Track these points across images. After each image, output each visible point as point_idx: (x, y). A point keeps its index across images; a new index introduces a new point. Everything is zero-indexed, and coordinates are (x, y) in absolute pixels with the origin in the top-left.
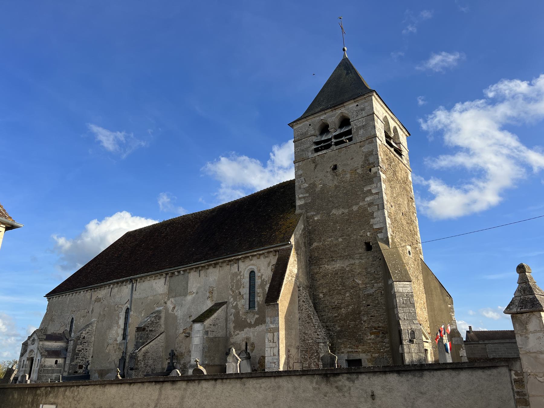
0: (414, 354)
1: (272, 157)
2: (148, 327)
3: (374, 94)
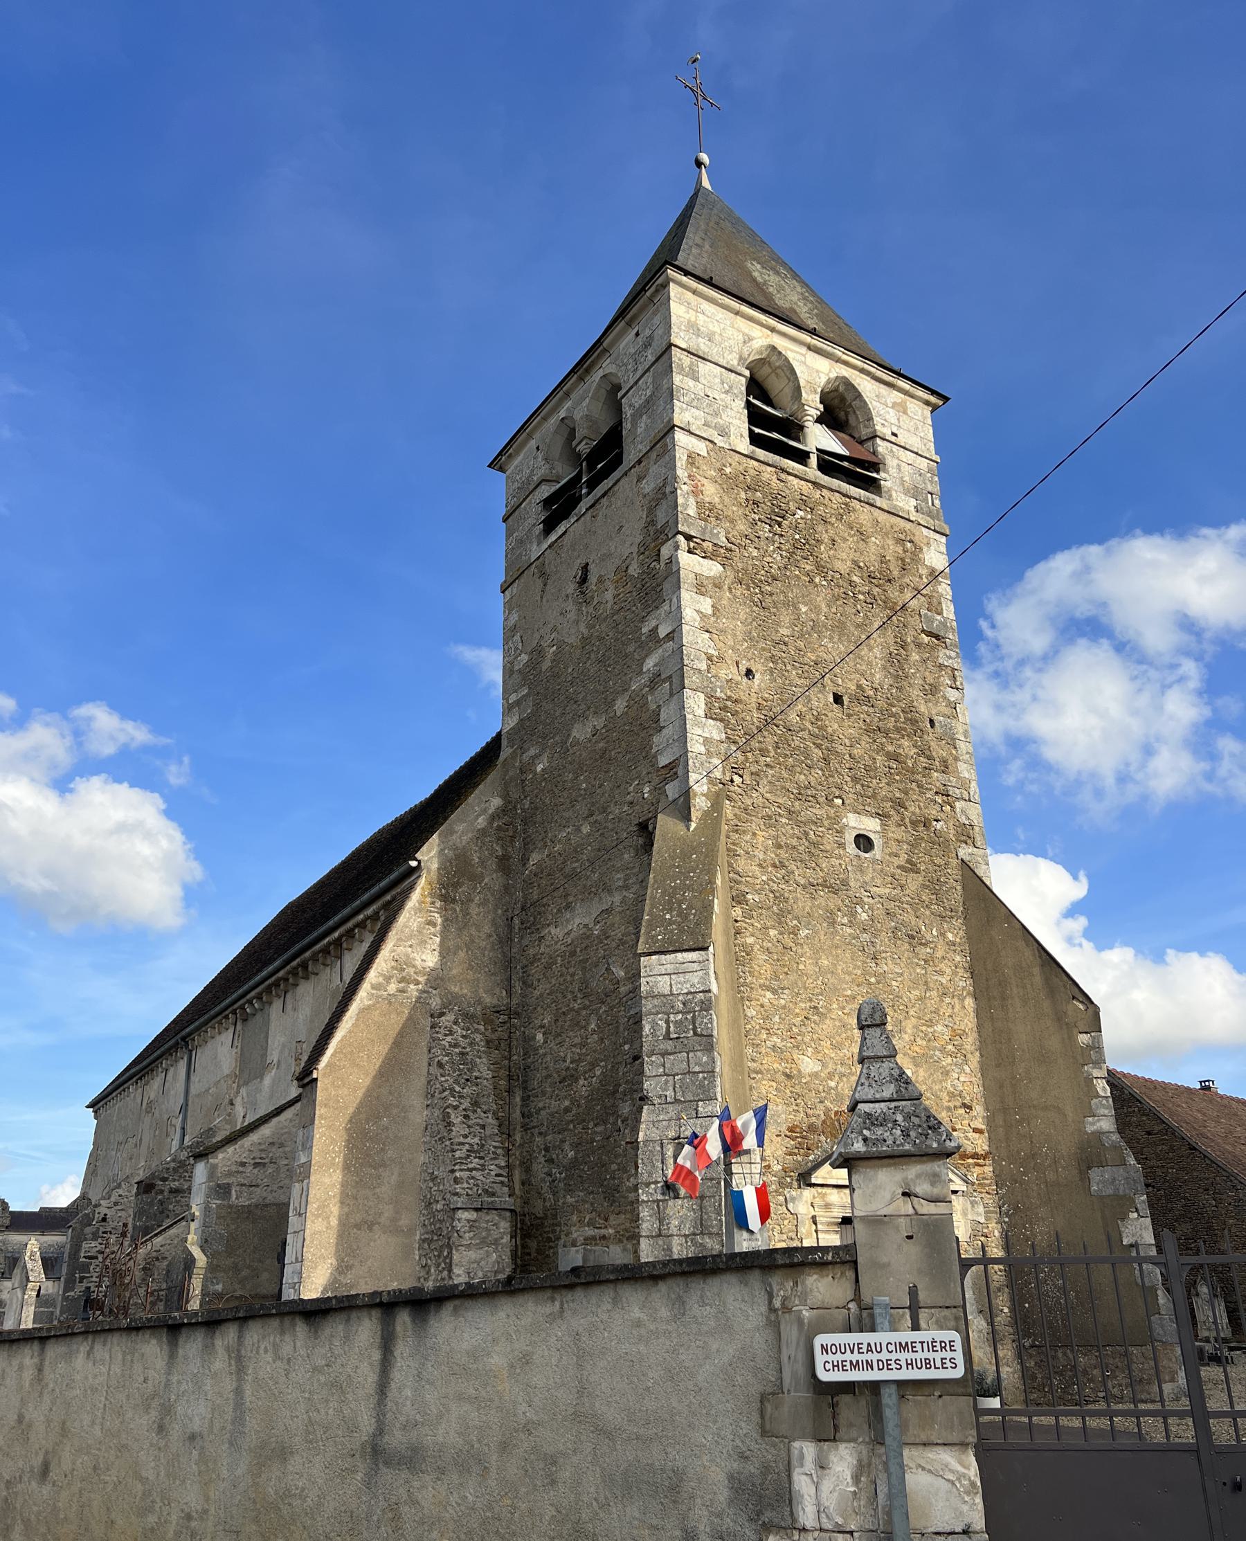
0: (676, 1241)
1: (989, 633)
2: (164, 1180)
3: (671, 272)
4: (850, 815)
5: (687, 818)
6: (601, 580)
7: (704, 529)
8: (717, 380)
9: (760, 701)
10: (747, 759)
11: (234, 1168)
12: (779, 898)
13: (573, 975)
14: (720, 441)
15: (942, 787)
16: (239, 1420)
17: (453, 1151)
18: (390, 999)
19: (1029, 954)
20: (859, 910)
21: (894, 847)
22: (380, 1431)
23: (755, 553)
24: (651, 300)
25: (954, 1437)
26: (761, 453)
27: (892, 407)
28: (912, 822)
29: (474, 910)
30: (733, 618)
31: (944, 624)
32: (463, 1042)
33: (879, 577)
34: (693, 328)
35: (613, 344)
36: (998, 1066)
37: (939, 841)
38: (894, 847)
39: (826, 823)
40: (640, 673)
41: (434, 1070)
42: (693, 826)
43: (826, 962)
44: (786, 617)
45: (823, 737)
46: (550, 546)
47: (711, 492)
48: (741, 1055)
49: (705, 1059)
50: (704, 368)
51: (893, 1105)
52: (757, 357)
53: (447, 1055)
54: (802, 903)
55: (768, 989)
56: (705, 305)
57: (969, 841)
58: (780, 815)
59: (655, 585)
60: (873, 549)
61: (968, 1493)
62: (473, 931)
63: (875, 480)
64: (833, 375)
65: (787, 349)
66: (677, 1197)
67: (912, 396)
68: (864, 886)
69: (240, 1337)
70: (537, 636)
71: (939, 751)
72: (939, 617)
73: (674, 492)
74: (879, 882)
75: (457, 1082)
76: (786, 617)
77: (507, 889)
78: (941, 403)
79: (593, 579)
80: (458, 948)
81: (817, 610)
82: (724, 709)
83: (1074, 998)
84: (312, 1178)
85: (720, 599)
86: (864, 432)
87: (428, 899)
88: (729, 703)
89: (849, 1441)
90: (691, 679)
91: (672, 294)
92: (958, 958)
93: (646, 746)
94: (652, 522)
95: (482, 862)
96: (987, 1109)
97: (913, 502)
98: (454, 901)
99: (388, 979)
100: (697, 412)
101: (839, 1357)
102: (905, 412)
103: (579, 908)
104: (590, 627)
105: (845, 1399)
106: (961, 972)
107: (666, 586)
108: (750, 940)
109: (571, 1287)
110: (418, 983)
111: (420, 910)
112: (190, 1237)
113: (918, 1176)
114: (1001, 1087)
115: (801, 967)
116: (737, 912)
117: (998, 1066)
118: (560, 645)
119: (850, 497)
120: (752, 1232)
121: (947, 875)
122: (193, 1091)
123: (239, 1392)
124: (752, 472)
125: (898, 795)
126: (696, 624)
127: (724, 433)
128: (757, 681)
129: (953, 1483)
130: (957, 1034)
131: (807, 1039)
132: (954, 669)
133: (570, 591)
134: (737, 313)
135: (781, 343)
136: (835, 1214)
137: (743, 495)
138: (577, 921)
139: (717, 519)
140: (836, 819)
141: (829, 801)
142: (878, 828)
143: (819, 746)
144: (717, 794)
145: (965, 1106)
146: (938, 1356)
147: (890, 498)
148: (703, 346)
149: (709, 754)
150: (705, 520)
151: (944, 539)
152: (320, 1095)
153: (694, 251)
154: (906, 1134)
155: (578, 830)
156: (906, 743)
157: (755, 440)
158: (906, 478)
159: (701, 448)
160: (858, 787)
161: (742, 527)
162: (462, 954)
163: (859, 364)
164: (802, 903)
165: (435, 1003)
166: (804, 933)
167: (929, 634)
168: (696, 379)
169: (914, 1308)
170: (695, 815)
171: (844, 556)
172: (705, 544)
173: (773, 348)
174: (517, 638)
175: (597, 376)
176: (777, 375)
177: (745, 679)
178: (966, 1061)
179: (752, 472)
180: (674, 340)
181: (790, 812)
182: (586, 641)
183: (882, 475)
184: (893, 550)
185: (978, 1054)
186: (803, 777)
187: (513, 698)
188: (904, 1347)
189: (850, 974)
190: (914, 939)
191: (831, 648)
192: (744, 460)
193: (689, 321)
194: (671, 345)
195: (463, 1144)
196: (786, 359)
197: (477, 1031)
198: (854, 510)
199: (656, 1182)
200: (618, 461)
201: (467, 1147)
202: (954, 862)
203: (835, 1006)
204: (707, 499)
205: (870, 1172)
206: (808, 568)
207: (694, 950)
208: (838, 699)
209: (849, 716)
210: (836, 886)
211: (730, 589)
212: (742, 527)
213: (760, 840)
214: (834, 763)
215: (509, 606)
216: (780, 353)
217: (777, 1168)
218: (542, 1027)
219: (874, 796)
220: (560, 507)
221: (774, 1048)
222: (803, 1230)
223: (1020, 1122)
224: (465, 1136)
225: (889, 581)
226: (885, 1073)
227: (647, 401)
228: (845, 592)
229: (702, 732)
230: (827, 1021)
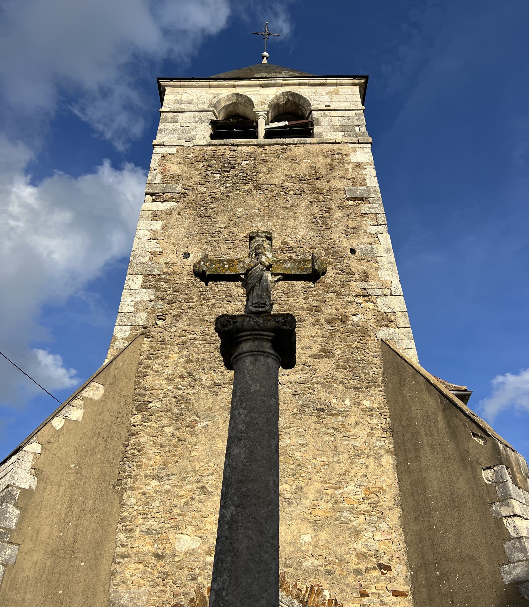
28: (327, 321)
37: (363, 331)
52: (228, 103)
55: (153, 477)
65: (245, 92)
67: (342, 85)
71: (356, 267)
88: (163, 277)
96: (411, 568)
106: (378, 433)
114: (421, 541)
115: (194, 453)
117: (416, 519)
124: (209, 152)
130: (372, 492)
132: (376, 214)
134: (210, 87)
135: (240, 91)
145: (381, 567)
149: (137, 310)
173: (237, 94)
178: (382, 518)
185: (398, 509)
190: (323, 411)
192: (205, 148)
196: (246, 97)
216: (241, 95)
221: (148, 531)
223: (439, 579)
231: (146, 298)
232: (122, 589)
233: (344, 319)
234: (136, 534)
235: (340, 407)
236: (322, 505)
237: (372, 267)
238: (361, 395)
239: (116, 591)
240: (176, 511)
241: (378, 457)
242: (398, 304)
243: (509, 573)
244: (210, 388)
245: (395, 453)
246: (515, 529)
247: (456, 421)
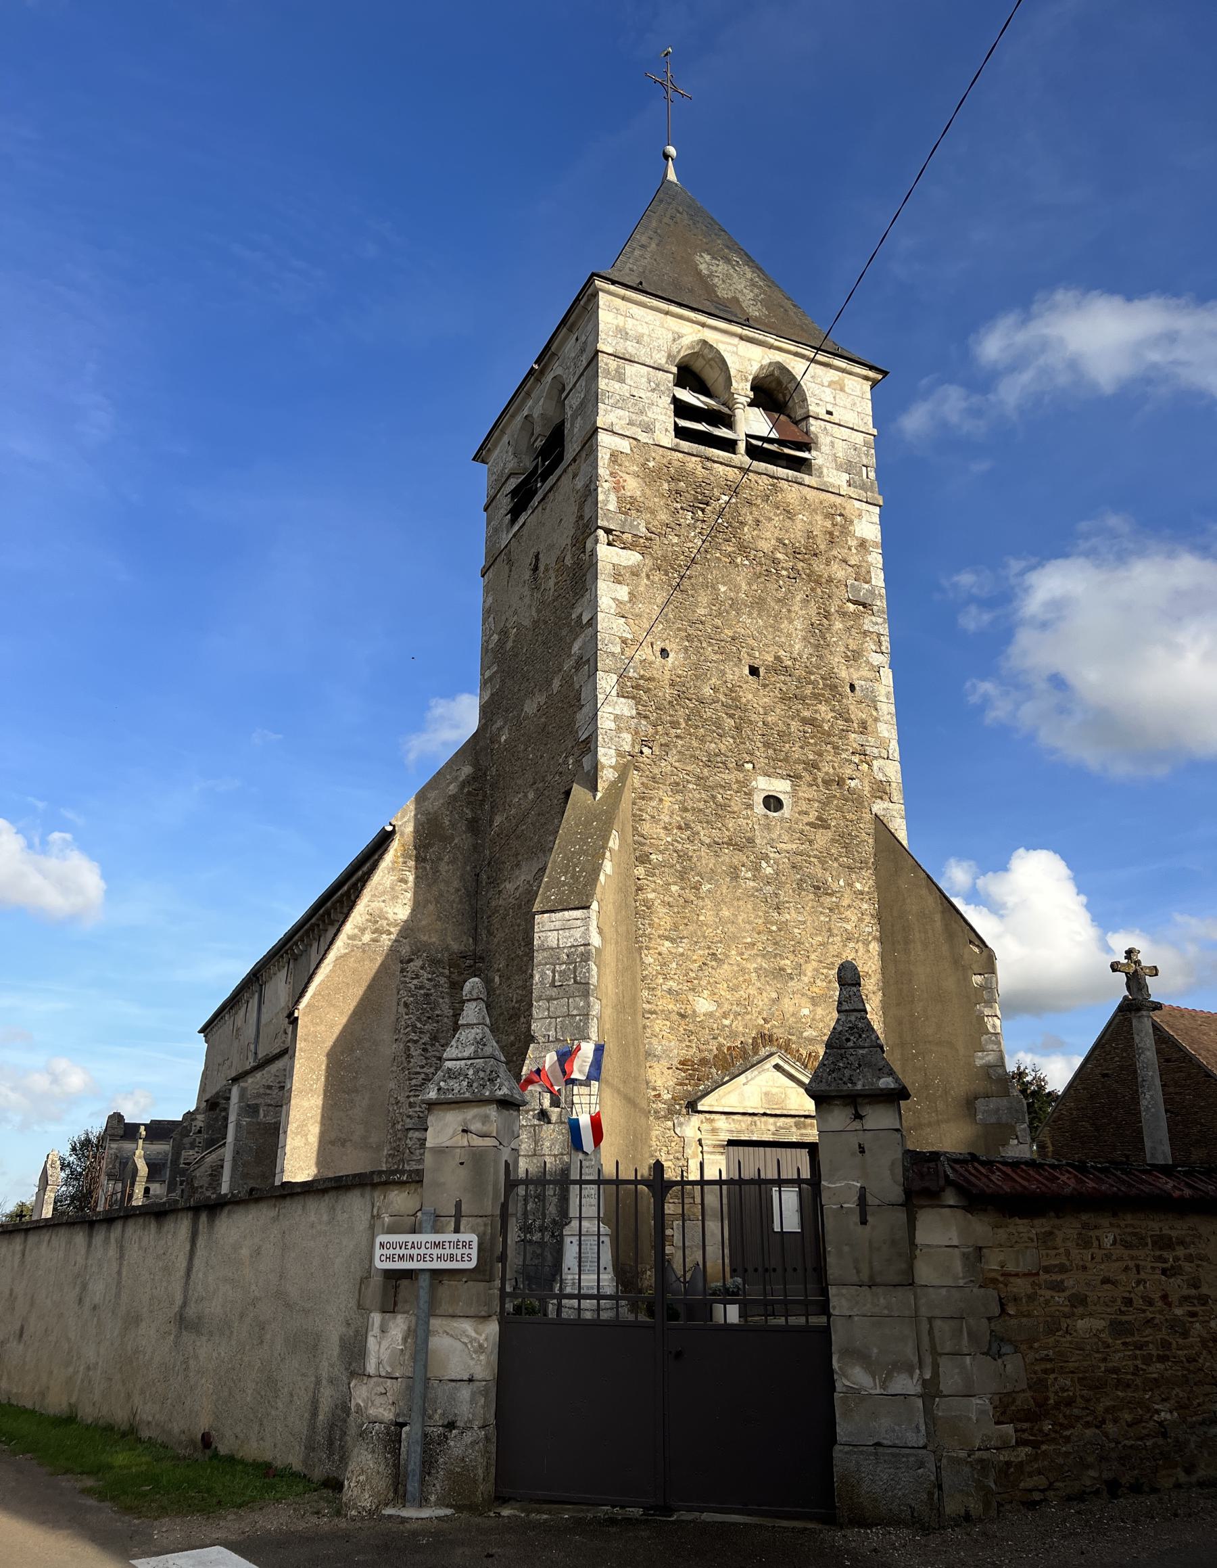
3: (598, 283)
4: (760, 778)
5: (594, 789)
6: (547, 570)
7: (624, 523)
8: (644, 380)
9: (674, 677)
10: (657, 733)
11: (262, 1091)
12: (683, 856)
13: (519, 925)
14: (644, 438)
15: (859, 748)
16: (118, 1295)
17: (410, 1079)
18: (364, 948)
19: (931, 901)
20: (764, 864)
21: (804, 806)
22: (185, 1304)
23: (675, 540)
24: (585, 308)
25: (472, 1312)
26: (685, 445)
27: (829, 386)
28: (824, 782)
29: (443, 867)
30: (650, 603)
31: (872, 592)
32: (428, 985)
33: (806, 552)
34: (623, 333)
35: (559, 348)
36: (898, 1005)
37: (856, 799)
38: (804, 806)
39: (735, 787)
40: (570, 656)
41: (402, 1010)
42: (599, 795)
43: (727, 913)
44: (704, 598)
45: (735, 706)
46: (514, 536)
47: (633, 486)
48: (634, 999)
49: (582, 1004)
50: (631, 369)
51: (470, 1062)
53: (412, 996)
54: (706, 860)
56: (635, 309)
57: (886, 797)
58: (688, 782)
59: (581, 576)
60: (799, 525)
61: (475, 1352)
62: (442, 886)
63: (805, 460)
64: (766, 362)
65: (718, 341)
66: (549, 1122)
67: (850, 373)
68: (771, 843)
69: (123, 1231)
70: (504, 618)
71: (857, 714)
72: (866, 586)
73: (596, 490)
74: (786, 839)
75: (419, 1019)
76: (704, 598)
77: (475, 848)
78: (880, 377)
79: (542, 568)
80: (428, 901)
81: (737, 588)
82: (637, 687)
83: (971, 942)
84: (293, 1102)
85: (637, 586)
86: (799, 413)
87: (401, 860)
88: (641, 682)
89: (404, 1313)
90: (603, 662)
91: (601, 303)
92: (865, 906)
93: (572, 721)
94: (581, 517)
95: (453, 825)
97: (846, 477)
98: (424, 860)
99: (363, 930)
100: (621, 412)
101: (391, 1251)
102: (842, 390)
103: (524, 868)
104: (539, 611)
105: (404, 1283)
106: (867, 919)
107: (589, 576)
108: (651, 896)
109: (284, 1197)
110: (390, 933)
111: (393, 869)
112: (137, 1152)
113: (474, 1117)
114: (900, 1023)
115: (702, 918)
116: (640, 871)
117: (898, 1005)
118: (518, 626)
119: (777, 478)
120: (586, 1154)
121: (859, 829)
122: (263, 1021)
123: (119, 1273)
124: (676, 463)
125: (811, 757)
126: (612, 611)
127: (648, 429)
128: (670, 660)
129: (465, 1344)
131: (704, 983)
132: (879, 635)
133: (527, 577)
134: (667, 313)
135: (711, 337)
136: (722, 1138)
137: (666, 486)
138: (523, 878)
139: (638, 511)
140: (743, 784)
141: (739, 767)
142: (789, 789)
143: (731, 716)
144: (625, 766)
146: (459, 1252)
147: (820, 475)
148: (630, 348)
149: (619, 729)
150: (626, 514)
151: (877, 510)
152: (301, 1031)
153: (637, 253)
154: (470, 1085)
155: (526, 796)
156: (823, 708)
157: (681, 433)
158: (840, 455)
159: (624, 446)
160: (770, 751)
161: (663, 516)
162: (431, 907)
163: (792, 348)
164: (706, 860)
165: (405, 951)
166: (706, 887)
167: (855, 603)
168: (622, 381)
169: (458, 1216)
170: (601, 785)
171: (768, 535)
172: (624, 536)
173: (705, 342)
174: (491, 619)
175: (549, 377)
176: (711, 367)
177: (659, 659)
179: (676, 463)
180: (600, 346)
181: (699, 778)
182: (535, 623)
183: (814, 453)
184: (821, 524)
185: (880, 993)
186: (713, 745)
187: (487, 674)
188: (436, 1245)
189: (750, 923)
190: (820, 889)
191: (749, 623)
193: (617, 327)
194: (598, 352)
195: (419, 1073)
197: (442, 974)
198: (782, 490)
199: (534, 1110)
200: (560, 458)
201: (423, 1076)
202: (867, 817)
203: (733, 952)
204: (629, 494)
205: (441, 1114)
206: (730, 549)
207: (578, 909)
208: (754, 671)
209: (765, 686)
210: (742, 843)
211: (648, 576)
212: (663, 517)
213: (667, 804)
214: (747, 731)
215: (487, 590)
217: (667, 1096)
218: (498, 970)
219: (786, 760)
220: (522, 499)
221: (670, 991)
222: (689, 1151)
223: (915, 1056)
224: (422, 1067)
225: (815, 555)
226: (471, 1037)
227: (581, 404)
228: (768, 568)
229: (613, 712)
230: (726, 966)
231: (627, 713)
232: (654, 1041)
233: (840, 783)
234: (659, 993)
235: (835, 887)
236: (819, 982)
237: (871, 715)
238: (854, 876)
239: (650, 1043)
240: (692, 975)
241: (866, 944)
242: (892, 771)
243: (982, 1058)
244: (709, 846)
245: (881, 941)
246: (994, 1026)
247: (954, 926)
